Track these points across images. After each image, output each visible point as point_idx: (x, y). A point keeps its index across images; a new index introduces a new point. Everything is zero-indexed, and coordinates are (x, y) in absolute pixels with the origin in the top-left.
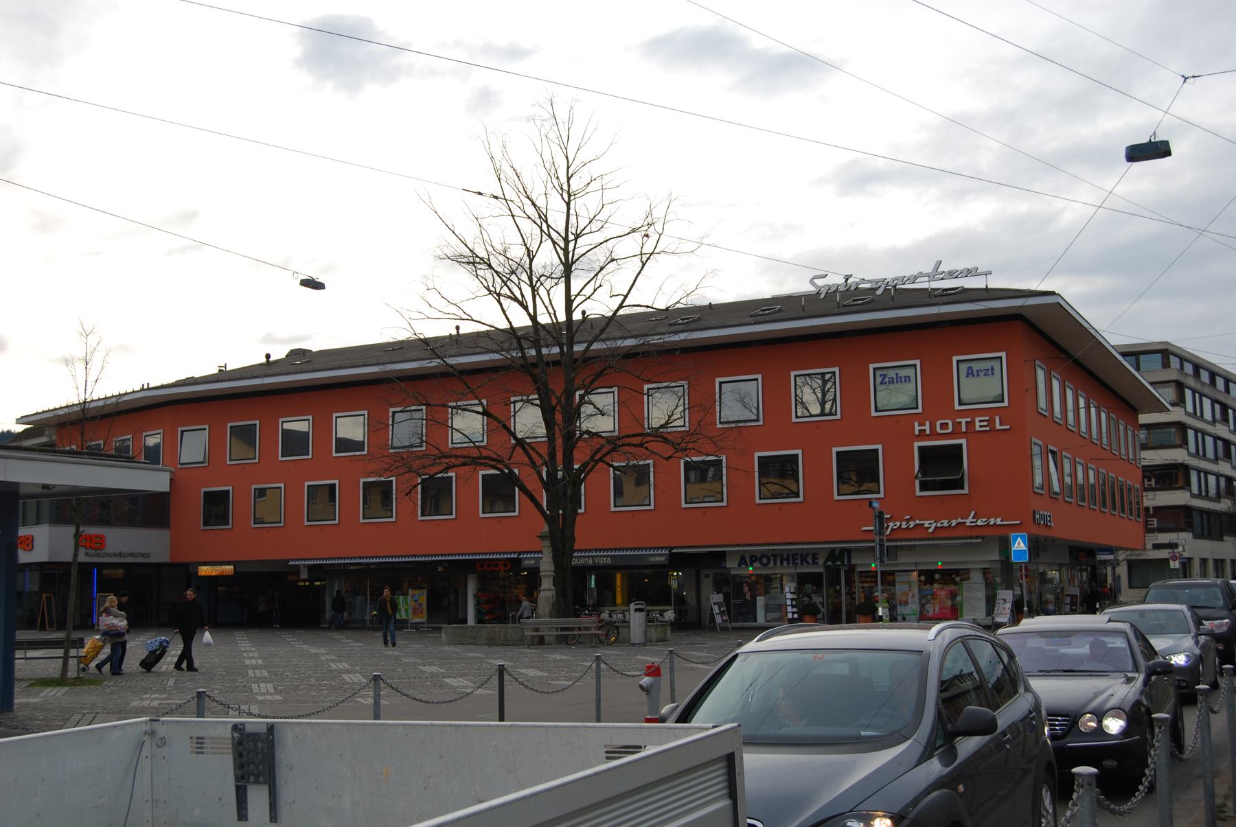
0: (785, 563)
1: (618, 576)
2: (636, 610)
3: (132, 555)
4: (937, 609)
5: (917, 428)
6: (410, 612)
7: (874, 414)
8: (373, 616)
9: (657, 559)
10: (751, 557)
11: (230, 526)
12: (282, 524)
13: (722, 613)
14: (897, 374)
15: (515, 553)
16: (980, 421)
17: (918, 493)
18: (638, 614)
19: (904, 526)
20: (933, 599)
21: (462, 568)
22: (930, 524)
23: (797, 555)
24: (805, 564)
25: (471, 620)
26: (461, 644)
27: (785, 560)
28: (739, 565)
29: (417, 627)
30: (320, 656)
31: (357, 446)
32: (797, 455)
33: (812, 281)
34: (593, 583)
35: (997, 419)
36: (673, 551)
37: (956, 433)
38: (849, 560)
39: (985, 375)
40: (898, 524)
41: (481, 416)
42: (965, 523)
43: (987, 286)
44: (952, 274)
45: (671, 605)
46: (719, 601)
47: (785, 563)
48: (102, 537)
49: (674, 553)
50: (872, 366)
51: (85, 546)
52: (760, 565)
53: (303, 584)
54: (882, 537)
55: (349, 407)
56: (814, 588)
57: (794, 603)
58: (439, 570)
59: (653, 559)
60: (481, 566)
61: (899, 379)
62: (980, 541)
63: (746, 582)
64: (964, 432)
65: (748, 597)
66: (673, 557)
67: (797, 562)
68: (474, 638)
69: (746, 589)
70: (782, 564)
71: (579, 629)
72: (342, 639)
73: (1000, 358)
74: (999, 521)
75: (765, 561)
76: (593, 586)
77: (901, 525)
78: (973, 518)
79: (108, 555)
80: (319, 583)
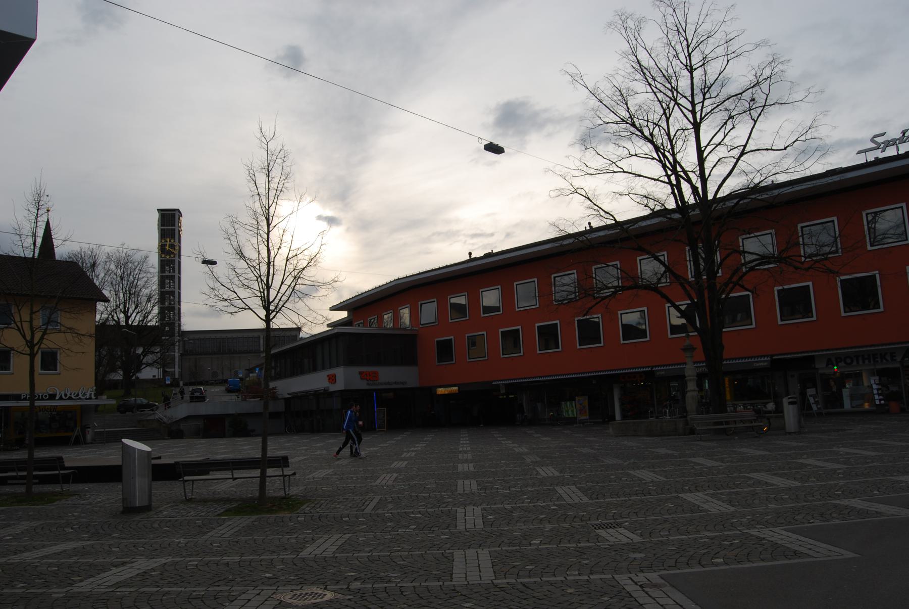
0: (867, 362)
1: (727, 379)
2: (790, 403)
3: (396, 383)
7: (517, 310)
9: (762, 364)
11: (454, 362)
12: (486, 358)
13: (817, 403)
15: (649, 367)
18: (791, 407)
21: (610, 380)
24: (884, 361)
25: (618, 416)
26: (625, 436)
28: (827, 365)
31: (496, 309)
32: (808, 286)
34: (707, 386)
36: (774, 358)
41: (745, 250)
43: (867, 160)
46: (813, 394)
47: (867, 362)
48: (376, 373)
49: (775, 359)
51: (367, 379)
52: (844, 365)
53: (502, 397)
55: (489, 285)
56: (890, 380)
57: (880, 392)
58: (594, 382)
59: (758, 365)
65: (834, 389)
69: (832, 383)
70: (864, 362)
71: (727, 423)
75: (849, 361)
76: (707, 388)
79: (381, 384)
80: (513, 396)
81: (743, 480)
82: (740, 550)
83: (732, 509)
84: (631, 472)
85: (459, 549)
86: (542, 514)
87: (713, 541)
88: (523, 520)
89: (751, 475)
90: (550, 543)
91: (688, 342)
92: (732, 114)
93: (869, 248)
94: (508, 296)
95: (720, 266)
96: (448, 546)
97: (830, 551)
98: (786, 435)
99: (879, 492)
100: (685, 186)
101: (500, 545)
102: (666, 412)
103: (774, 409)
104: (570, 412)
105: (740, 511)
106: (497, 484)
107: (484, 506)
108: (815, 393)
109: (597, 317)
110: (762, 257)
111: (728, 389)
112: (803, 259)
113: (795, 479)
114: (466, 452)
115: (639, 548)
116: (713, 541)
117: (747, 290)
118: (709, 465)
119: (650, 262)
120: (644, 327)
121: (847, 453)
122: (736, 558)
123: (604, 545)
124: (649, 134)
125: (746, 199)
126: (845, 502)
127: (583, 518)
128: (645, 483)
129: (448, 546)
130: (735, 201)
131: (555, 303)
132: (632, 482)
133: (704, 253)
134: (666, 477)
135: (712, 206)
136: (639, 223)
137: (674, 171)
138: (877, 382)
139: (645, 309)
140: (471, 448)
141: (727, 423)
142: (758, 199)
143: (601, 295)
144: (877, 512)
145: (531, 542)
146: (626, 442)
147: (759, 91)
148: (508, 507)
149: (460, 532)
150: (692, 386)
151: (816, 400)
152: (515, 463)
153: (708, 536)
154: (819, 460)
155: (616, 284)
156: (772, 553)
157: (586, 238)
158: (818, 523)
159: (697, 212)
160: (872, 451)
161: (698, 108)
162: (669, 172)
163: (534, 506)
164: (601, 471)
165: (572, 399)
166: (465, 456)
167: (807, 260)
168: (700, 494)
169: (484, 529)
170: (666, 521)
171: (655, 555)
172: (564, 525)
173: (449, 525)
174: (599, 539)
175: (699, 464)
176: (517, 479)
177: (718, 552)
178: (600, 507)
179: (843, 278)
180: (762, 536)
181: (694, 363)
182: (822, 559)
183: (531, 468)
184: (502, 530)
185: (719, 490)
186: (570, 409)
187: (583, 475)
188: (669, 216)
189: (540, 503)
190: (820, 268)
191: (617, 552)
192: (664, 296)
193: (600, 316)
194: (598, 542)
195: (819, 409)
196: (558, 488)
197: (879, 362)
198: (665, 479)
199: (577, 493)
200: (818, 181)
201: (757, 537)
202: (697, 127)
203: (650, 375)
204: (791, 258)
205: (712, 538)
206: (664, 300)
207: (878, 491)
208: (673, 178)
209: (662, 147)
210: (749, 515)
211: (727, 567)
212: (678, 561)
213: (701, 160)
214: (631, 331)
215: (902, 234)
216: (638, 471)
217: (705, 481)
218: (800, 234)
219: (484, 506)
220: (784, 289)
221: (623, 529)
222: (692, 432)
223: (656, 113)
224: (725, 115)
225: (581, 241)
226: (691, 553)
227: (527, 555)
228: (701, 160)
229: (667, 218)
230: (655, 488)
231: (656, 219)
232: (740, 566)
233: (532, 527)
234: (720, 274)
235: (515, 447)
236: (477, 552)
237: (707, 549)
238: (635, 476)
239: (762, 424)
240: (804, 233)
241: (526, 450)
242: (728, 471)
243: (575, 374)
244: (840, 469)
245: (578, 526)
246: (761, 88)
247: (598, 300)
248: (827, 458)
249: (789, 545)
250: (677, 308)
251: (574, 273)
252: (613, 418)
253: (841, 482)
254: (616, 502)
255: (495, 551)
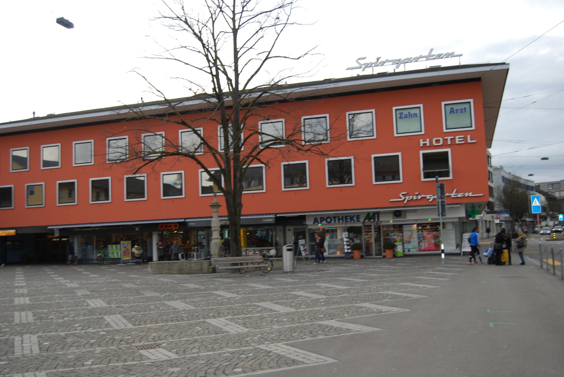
0: (341, 221)
2: (289, 250)
4: (427, 245)
5: (422, 143)
6: (123, 254)
7: (396, 135)
8: (98, 257)
9: (268, 220)
10: (321, 218)
13: (305, 250)
14: (409, 112)
15: (182, 219)
16: (459, 138)
17: (423, 179)
18: (289, 252)
19: (415, 198)
20: (424, 239)
22: (430, 197)
23: (347, 216)
24: (352, 221)
26: (161, 273)
27: (341, 219)
28: (314, 222)
29: (125, 262)
30: (76, 291)
31: (55, 163)
33: (357, 61)
35: (469, 137)
37: (445, 145)
38: (378, 219)
39: (461, 112)
40: (411, 197)
42: (451, 196)
44: (439, 56)
45: (273, 246)
50: (394, 108)
54: (443, 200)
55: (50, 142)
56: (355, 235)
59: (266, 220)
60: (162, 227)
61: (410, 115)
62: (459, 206)
63: (316, 233)
64: (449, 145)
66: (277, 219)
67: (347, 220)
68: (169, 270)
69: (316, 236)
70: (339, 222)
71: (241, 264)
72: (83, 271)
73: (469, 102)
74: (470, 194)
75: (329, 220)
77: (413, 198)
78: (456, 193)
80: (65, 239)
81: (253, 307)
82: (254, 361)
83: (246, 330)
84: (167, 303)
85: (17, 373)
86: (92, 338)
87: (234, 355)
88: (76, 344)
89: (260, 304)
90: (100, 363)
91: (215, 200)
92: (262, 27)
93: (349, 139)
94: (66, 153)
95: (243, 145)
96: (7, 370)
97: (317, 358)
98: (283, 274)
99: (349, 315)
100: (222, 77)
101: (56, 367)
102: (193, 255)
103: (275, 255)
104: (115, 254)
105: (252, 332)
106: (52, 315)
107: (40, 334)
108: (304, 243)
109: (142, 177)
110: (277, 139)
111: (242, 238)
112: (303, 143)
113: (291, 306)
114: (21, 287)
115: (176, 363)
116: (234, 355)
117: (262, 163)
118: (228, 297)
119: (190, 134)
120: (179, 187)
121: (326, 287)
122: (252, 367)
123: (147, 362)
124: (198, 31)
125: (267, 93)
126: (326, 323)
127: (128, 341)
128: (179, 312)
129: (7, 370)
130: (259, 94)
131: (108, 162)
132: (168, 311)
133: (232, 130)
134: (195, 306)
135: (241, 96)
136: (184, 102)
137: (215, 64)
138: (347, 236)
139: (183, 172)
140: (27, 284)
141: (241, 264)
142: (276, 94)
143: (149, 158)
144: (348, 330)
145: (84, 363)
146: (162, 279)
147: (283, 12)
148: (63, 334)
149: (18, 358)
150: (216, 235)
151: (305, 248)
152: (68, 296)
153: (230, 352)
154: (307, 292)
155: (161, 150)
156: (277, 363)
157: (140, 110)
158: (308, 338)
159: (230, 98)
160: (343, 285)
161: (237, 17)
162: (211, 65)
163: (85, 332)
164: (143, 302)
165: (117, 243)
166: (21, 291)
167: (307, 144)
168: (222, 319)
169: (41, 354)
170: (196, 341)
171: (189, 368)
172: (112, 347)
173: (7, 352)
174: (143, 358)
175: (220, 296)
176: (70, 310)
177: (238, 364)
178: (142, 332)
179: (331, 159)
180: (270, 350)
181: (219, 217)
182: (322, 363)
183: (81, 301)
184: (57, 354)
185: (236, 315)
186: (114, 251)
187: (127, 305)
188: (207, 99)
189: (91, 330)
190: (315, 150)
191: (158, 368)
192: (199, 163)
193: (145, 175)
194: (142, 360)
195: (307, 255)
196: (106, 317)
197: (349, 222)
198: (194, 308)
199: (123, 321)
200: (319, 86)
201: (266, 351)
202: (235, 31)
203: (183, 225)
204: (296, 141)
205: (233, 353)
206: (199, 166)
207: (347, 314)
208: (214, 70)
209: (207, 44)
210: (259, 334)
211: (245, 375)
212: (207, 373)
213: (236, 59)
214: (169, 189)
215: (370, 131)
216: (172, 302)
217: (225, 309)
218: (303, 124)
219: (40, 334)
220: (289, 165)
221: (161, 348)
222: (214, 271)
223: (205, 16)
224: (258, 27)
225: (136, 112)
226: (217, 365)
227: (81, 374)
228: (236, 59)
229: (206, 101)
230: (186, 315)
231: (198, 101)
232: (254, 373)
233: (84, 350)
234: (242, 149)
235: (66, 282)
236: (35, 374)
237: (229, 361)
238: (170, 306)
239: (266, 265)
240: (306, 124)
241: (77, 285)
242: (242, 301)
243: (139, 221)
244: (322, 299)
245: (124, 348)
246: (284, 10)
247: (147, 162)
248: (313, 291)
249: (288, 356)
250: (209, 172)
251: (125, 138)
252: (151, 259)
253: (323, 308)
254: (156, 327)
255: (52, 373)
